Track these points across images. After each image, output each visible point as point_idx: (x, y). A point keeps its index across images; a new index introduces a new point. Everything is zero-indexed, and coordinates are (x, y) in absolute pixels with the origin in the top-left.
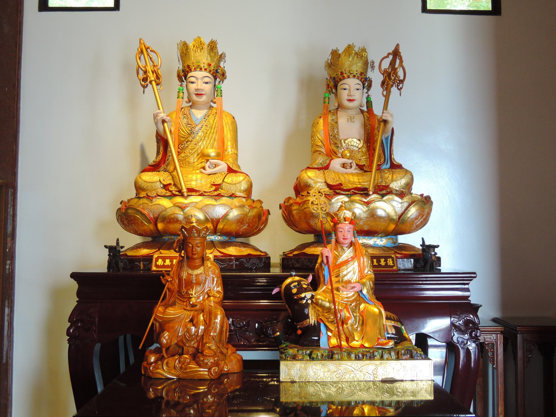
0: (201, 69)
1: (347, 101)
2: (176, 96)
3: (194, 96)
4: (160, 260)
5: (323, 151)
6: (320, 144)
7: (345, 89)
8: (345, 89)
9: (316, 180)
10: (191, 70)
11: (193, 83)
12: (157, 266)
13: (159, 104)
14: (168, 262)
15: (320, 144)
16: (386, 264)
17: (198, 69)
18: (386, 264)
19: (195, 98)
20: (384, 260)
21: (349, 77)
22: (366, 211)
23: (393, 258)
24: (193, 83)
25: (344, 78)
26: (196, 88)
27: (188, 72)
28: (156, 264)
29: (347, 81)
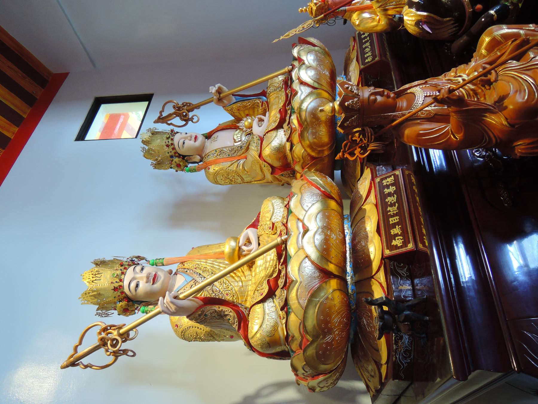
0: (123, 273)
1: (196, 143)
2: (207, 131)
3: (155, 286)
4: (394, 243)
5: (242, 162)
6: (236, 164)
7: (184, 143)
8: (184, 143)
9: (263, 319)
10: (120, 286)
11: (137, 286)
12: (405, 244)
13: (158, 331)
14: (397, 230)
15: (236, 164)
16: (392, 185)
17: (123, 277)
18: (392, 185)
19: (158, 286)
20: (386, 190)
21: (172, 139)
22: (318, 277)
23: (382, 180)
24: (137, 286)
25: (172, 144)
26: (145, 280)
27: (122, 293)
28: (401, 247)
29: (176, 142)
